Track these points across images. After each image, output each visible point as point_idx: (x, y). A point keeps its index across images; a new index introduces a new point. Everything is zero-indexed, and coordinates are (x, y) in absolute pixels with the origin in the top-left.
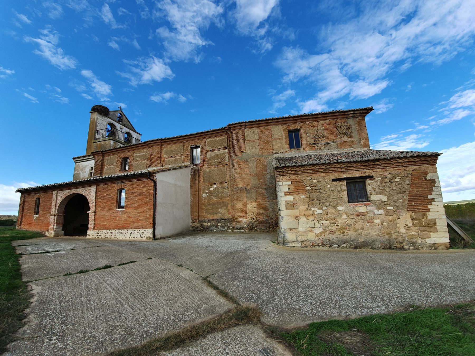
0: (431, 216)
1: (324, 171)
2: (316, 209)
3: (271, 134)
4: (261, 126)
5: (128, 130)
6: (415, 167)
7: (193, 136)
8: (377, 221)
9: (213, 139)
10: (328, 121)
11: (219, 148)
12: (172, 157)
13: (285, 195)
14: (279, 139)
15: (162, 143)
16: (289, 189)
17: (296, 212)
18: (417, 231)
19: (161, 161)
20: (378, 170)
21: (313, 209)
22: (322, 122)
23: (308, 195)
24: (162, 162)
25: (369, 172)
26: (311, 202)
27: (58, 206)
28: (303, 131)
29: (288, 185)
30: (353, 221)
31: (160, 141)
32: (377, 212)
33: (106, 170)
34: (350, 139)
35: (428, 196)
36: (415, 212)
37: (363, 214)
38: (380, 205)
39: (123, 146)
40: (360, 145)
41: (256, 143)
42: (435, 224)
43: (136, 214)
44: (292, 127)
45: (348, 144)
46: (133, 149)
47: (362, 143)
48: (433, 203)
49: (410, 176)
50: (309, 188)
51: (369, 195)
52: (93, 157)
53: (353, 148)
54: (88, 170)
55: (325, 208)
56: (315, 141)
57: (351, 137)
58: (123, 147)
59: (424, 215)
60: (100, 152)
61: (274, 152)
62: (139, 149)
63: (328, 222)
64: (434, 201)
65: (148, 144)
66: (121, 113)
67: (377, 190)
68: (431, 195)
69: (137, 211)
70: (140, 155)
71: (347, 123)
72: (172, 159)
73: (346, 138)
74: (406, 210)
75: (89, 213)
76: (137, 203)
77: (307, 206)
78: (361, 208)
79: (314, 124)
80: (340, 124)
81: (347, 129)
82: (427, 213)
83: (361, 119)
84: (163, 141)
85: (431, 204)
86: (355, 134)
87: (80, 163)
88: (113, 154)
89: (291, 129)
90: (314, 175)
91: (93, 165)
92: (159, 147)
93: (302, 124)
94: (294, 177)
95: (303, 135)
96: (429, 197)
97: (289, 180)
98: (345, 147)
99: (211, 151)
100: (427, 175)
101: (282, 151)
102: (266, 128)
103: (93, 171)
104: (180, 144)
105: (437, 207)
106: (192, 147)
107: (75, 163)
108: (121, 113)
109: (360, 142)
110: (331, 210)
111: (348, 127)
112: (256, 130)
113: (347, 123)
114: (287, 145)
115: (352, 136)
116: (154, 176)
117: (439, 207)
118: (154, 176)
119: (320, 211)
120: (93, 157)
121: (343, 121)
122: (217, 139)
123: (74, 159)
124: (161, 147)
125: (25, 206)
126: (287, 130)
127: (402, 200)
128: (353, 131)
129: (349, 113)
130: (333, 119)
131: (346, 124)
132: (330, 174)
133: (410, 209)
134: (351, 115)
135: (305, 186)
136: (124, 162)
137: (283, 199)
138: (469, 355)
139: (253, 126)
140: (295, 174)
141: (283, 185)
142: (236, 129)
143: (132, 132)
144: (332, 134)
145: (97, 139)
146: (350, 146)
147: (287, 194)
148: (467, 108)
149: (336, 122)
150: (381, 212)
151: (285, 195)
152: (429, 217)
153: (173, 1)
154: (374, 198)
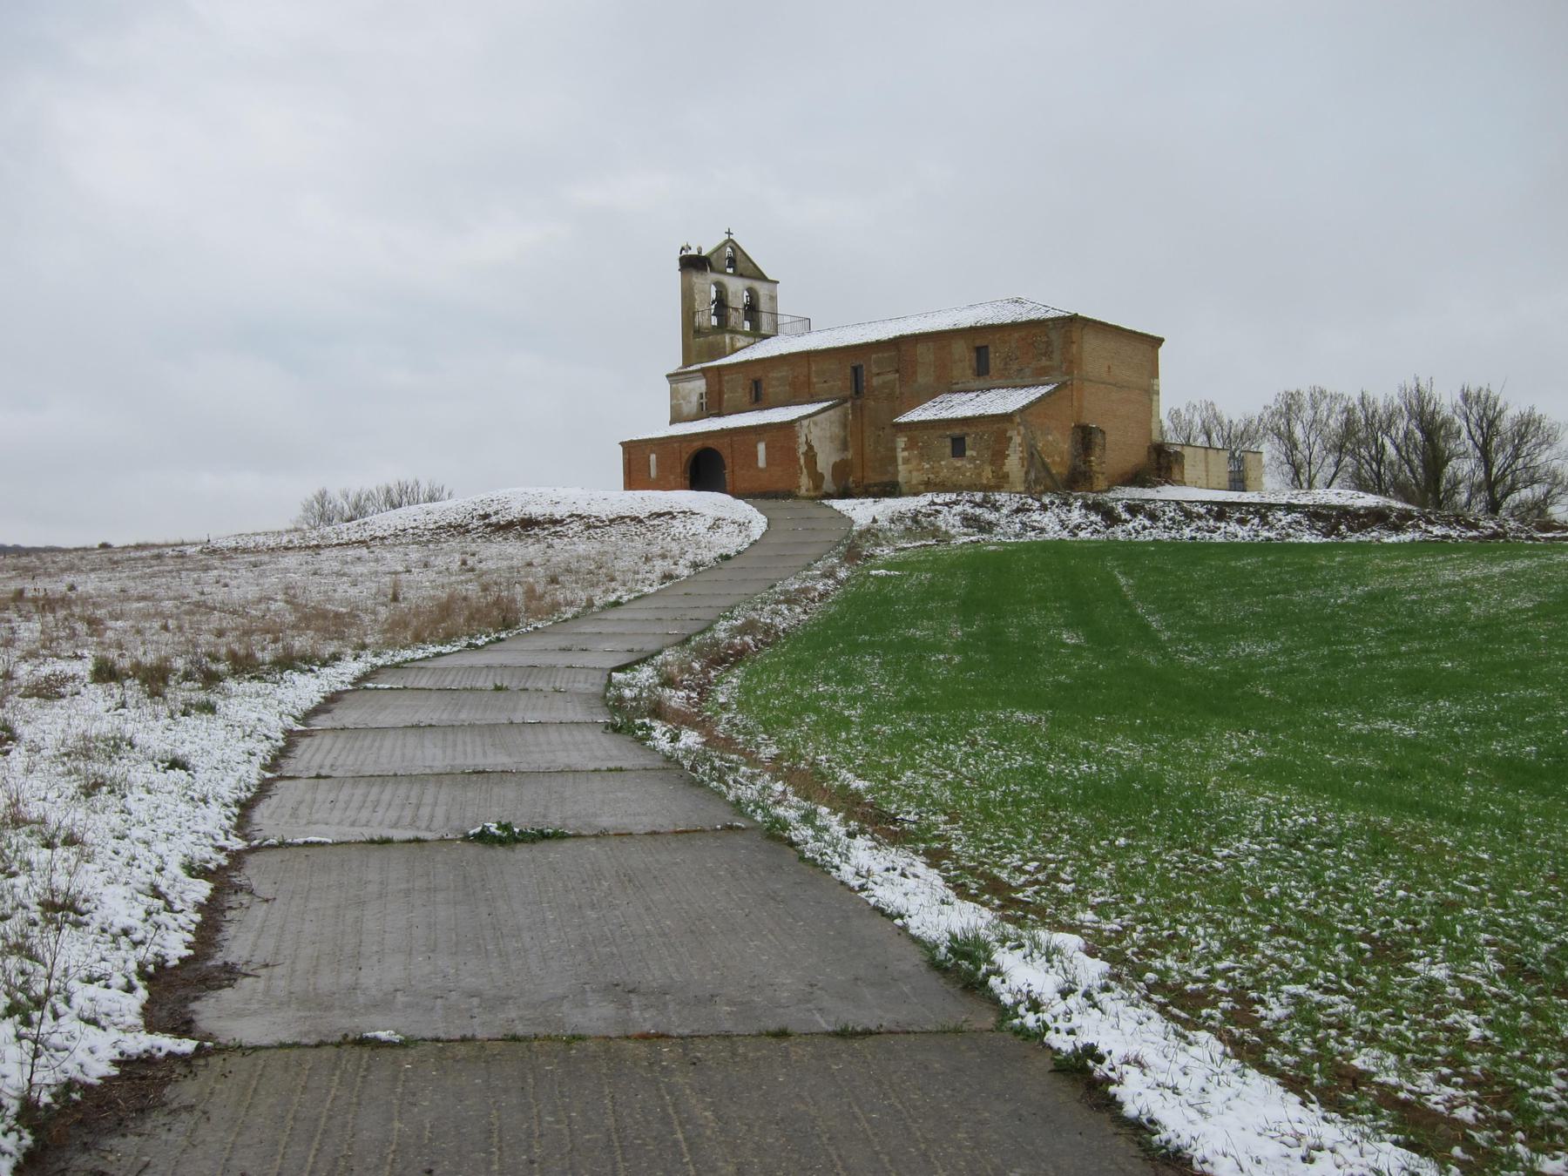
0: (1006, 469)
17: (910, 467)
22: (1016, 335)
25: (966, 429)
26: (921, 457)
28: (991, 349)
37: (958, 468)
38: (972, 459)
44: (979, 343)
51: (124, 1058)
54: (695, 399)
56: (1006, 364)
57: (1051, 359)
70: (779, 375)
73: (1044, 362)
78: (959, 464)
86: (1057, 356)
91: (703, 389)
95: (991, 356)
103: (704, 401)
110: (936, 465)
111: (1049, 344)
112: (931, 344)
123: (668, 376)
127: (987, 455)
138: (573, 1174)
147: (904, 450)
148: (1278, 1076)
149: (1035, 335)
154: (968, 453)
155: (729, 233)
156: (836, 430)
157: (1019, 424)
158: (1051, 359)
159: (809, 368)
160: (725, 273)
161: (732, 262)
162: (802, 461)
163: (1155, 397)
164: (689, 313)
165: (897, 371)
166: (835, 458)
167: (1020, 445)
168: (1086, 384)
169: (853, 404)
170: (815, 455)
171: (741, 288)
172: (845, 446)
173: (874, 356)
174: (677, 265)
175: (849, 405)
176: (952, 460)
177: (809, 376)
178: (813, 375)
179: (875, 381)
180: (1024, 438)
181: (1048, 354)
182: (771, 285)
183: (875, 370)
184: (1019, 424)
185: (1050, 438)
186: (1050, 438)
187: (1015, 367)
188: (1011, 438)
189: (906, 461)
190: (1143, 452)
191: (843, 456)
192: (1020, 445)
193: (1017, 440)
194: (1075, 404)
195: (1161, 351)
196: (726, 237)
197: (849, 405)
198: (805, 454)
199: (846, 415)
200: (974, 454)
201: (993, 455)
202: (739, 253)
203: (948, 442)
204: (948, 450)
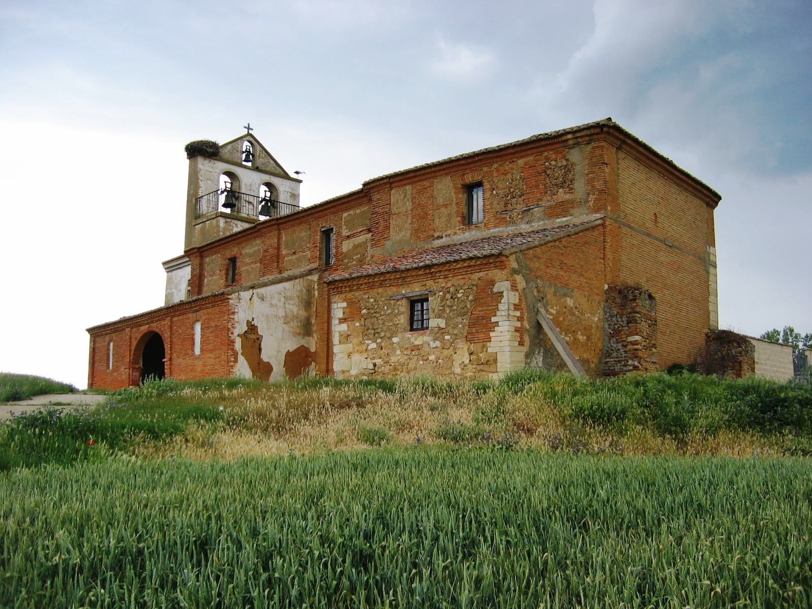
0: (492, 348)
1: (381, 286)
2: (370, 342)
3: (432, 196)
4: (417, 182)
5: (267, 178)
6: (481, 274)
7: (320, 209)
8: (432, 357)
9: (352, 212)
10: (531, 158)
11: (359, 230)
12: (294, 253)
13: (340, 323)
14: (446, 206)
15: (279, 225)
16: (344, 313)
17: (349, 347)
18: (474, 370)
19: (278, 262)
20: (440, 280)
21: (367, 342)
22: (521, 162)
23: (362, 323)
24: (281, 266)
27: (132, 353)
29: (344, 308)
30: (406, 358)
31: (388, 180)
32: (433, 345)
33: (207, 285)
34: (568, 197)
35: (492, 318)
36: (474, 343)
37: (418, 348)
39: (253, 225)
40: (586, 209)
41: (407, 217)
42: (495, 361)
43: (212, 360)
45: (562, 209)
46: (241, 240)
47: (591, 204)
48: (496, 328)
49: (475, 288)
50: (364, 311)
52: (188, 259)
53: (571, 215)
55: (379, 341)
58: (253, 228)
59: (484, 346)
60: (196, 250)
61: (436, 235)
62: (249, 240)
63: (380, 360)
64: (516, 327)
65: (259, 230)
66: (251, 139)
67: (436, 311)
68: (496, 316)
69: (212, 356)
70: (251, 251)
71: (567, 160)
72: (294, 257)
73: (562, 195)
74: (464, 340)
75: (164, 362)
76: (213, 343)
77: (361, 339)
79: (507, 166)
80: (553, 163)
81: (565, 176)
82: (488, 344)
83: (597, 147)
84: (281, 221)
85: (494, 331)
86: (580, 186)
87: (174, 272)
88: (216, 253)
89: (467, 181)
90: (371, 291)
92: (276, 233)
93: (485, 169)
94: (349, 295)
96: (494, 319)
97: (344, 300)
98: (558, 216)
99: (348, 237)
100: (494, 285)
101: (449, 232)
102: (426, 184)
104: (305, 226)
105: (500, 334)
106: (323, 230)
107: (167, 272)
108: (251, 139)
109: (587, 202)
111: (568, 169)
113: (567, 160)
114: (459, 219)
115: (573, 189)
116: (229, 299)
117: (502, 334)
118: (229, 299)
119: (374, 345)
120: (188, 259)
121: (560, 156)
122: (358, 211)
123: (164, 264)
124: (279, 234)
125: (96, 355)
126: (460, 186)
128: (577, 177)
129: (564, 138)
130: (541, 153)
131: (565, 163)
132: (388, 289)
133: (469, 339)
134: (571, 142)
135: (360, 309)
136: (231, 266)
137: (338, 328)
139: (404, 182)
140: (351, 291)
141: (338, 308)
142: (379, 192)
143: (276, 181)
144: (537, 186)
145: (199, 217)
146: (565, 213)
147: (342, 321)
149: (547, 159)
150: (438, 343)
151: (340, 323)
152: (490, 350)
153: (0, 421)
154: (434, 323)
155: (249, 128)
156: (295, 308)
157: (515, 272)
158: (571, 190)
159: (279, 239)
160: (241, 166)
161: (249, 155)
162: (238, 345)
163: (711, 270)
164: (194, 200)
165: (369, 230)
166: (292, 345)
167: (517, 307)
168: (625, 230)
169: (320, 278)
170: (259, 339)
171: (258, 182)
172: (306, 329)
173: (345, 215)
174: (185, 154)
175: (315, 277)
176: (408, 335)
177: (278, 248)
178: (283, 246)
179: (346, 246)
180: (523, 295)
181: (566, 183)
182: (297, 183)
183: (345, 232)
184: (515, 272)
185: (570, 302)
186: (570, 302)
187: (521, 207)
188: (500, 294)
189: (346, 338)
190: (701, 340)
191: (303, 342)
192: (517, 307)
193: (510, 298)
194: (609, 255)
195: (717, 212)
196: (245, 132)
197: (315, 277)
198: (244, 336)
199: (309, 291)
200: (442, 323)
201: (470, 326)
202: (258, 148)
203: (404, 306)
204: (403, 320)
